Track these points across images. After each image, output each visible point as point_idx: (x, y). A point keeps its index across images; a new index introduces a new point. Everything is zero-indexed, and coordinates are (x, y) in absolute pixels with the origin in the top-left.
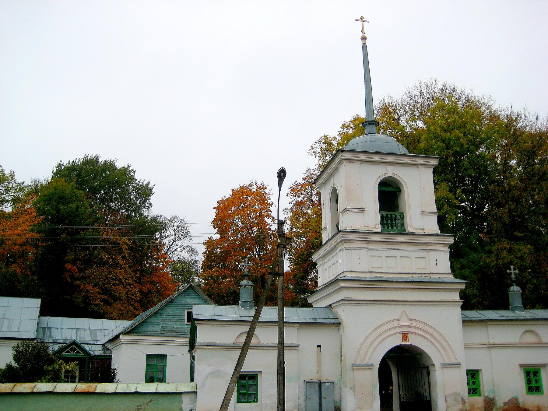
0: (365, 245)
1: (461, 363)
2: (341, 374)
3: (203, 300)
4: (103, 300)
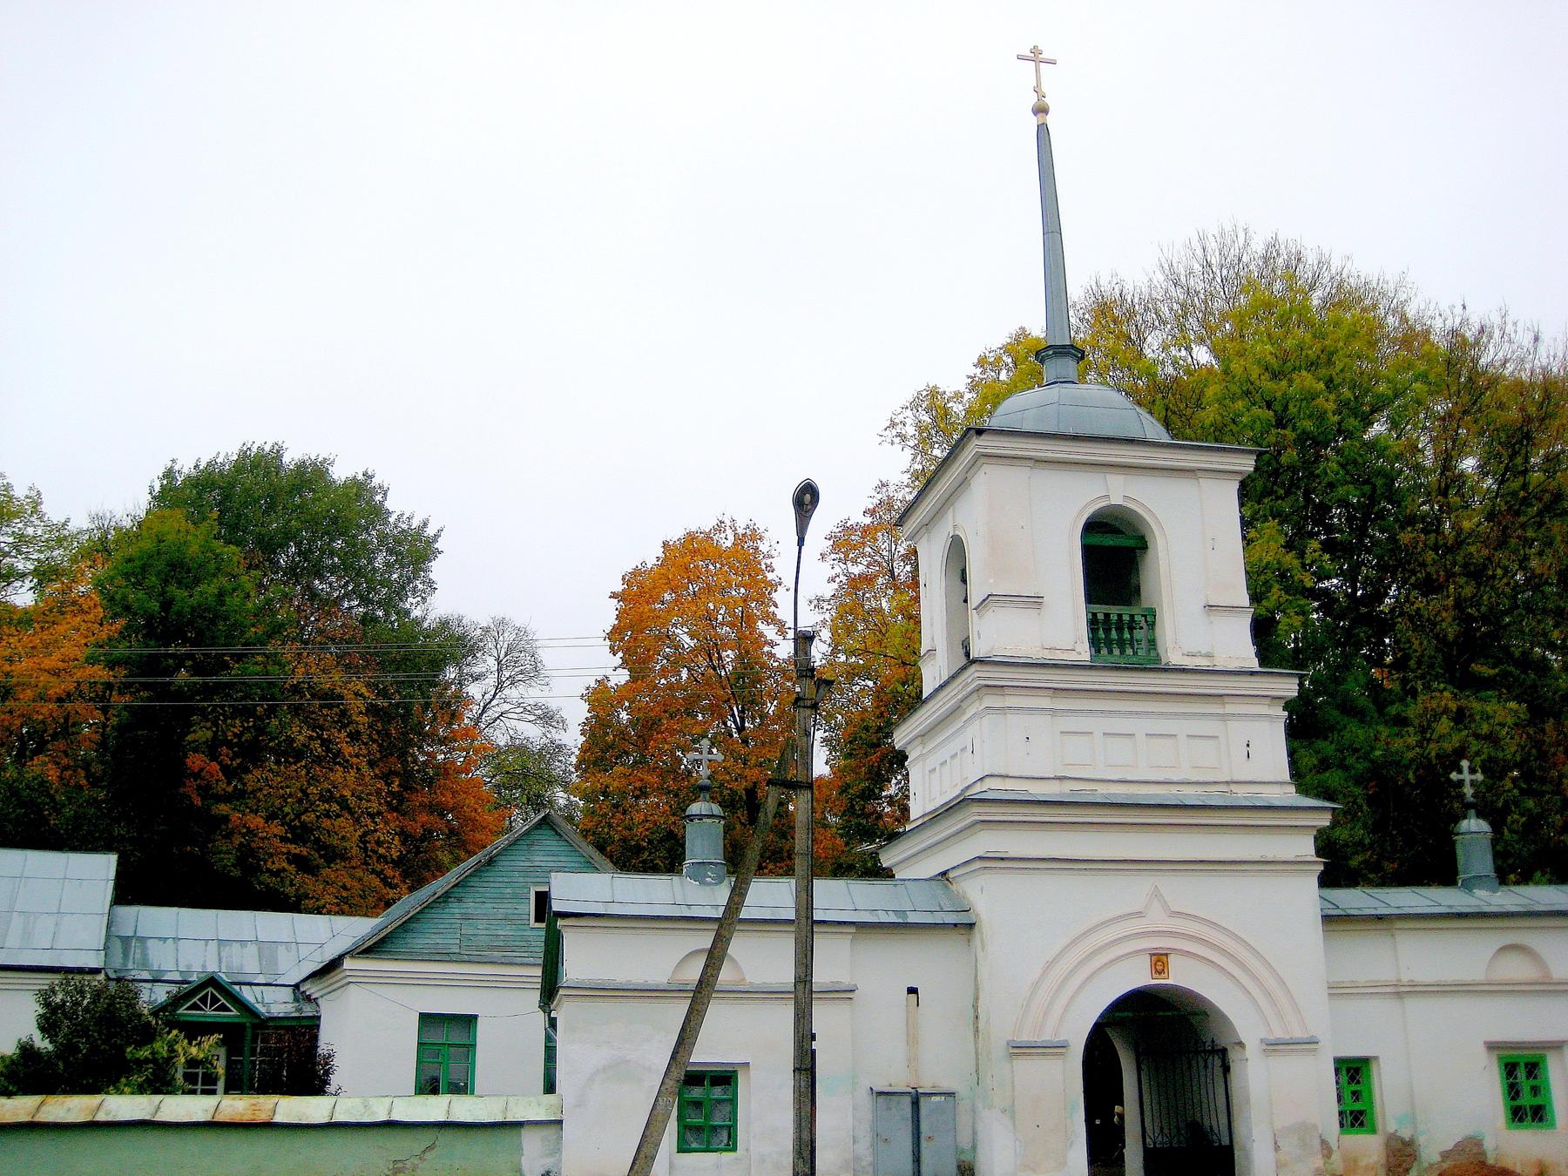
0: (1045, 702)
1: (1320, 1038)
3: (582, 860)
4: (297, 860)
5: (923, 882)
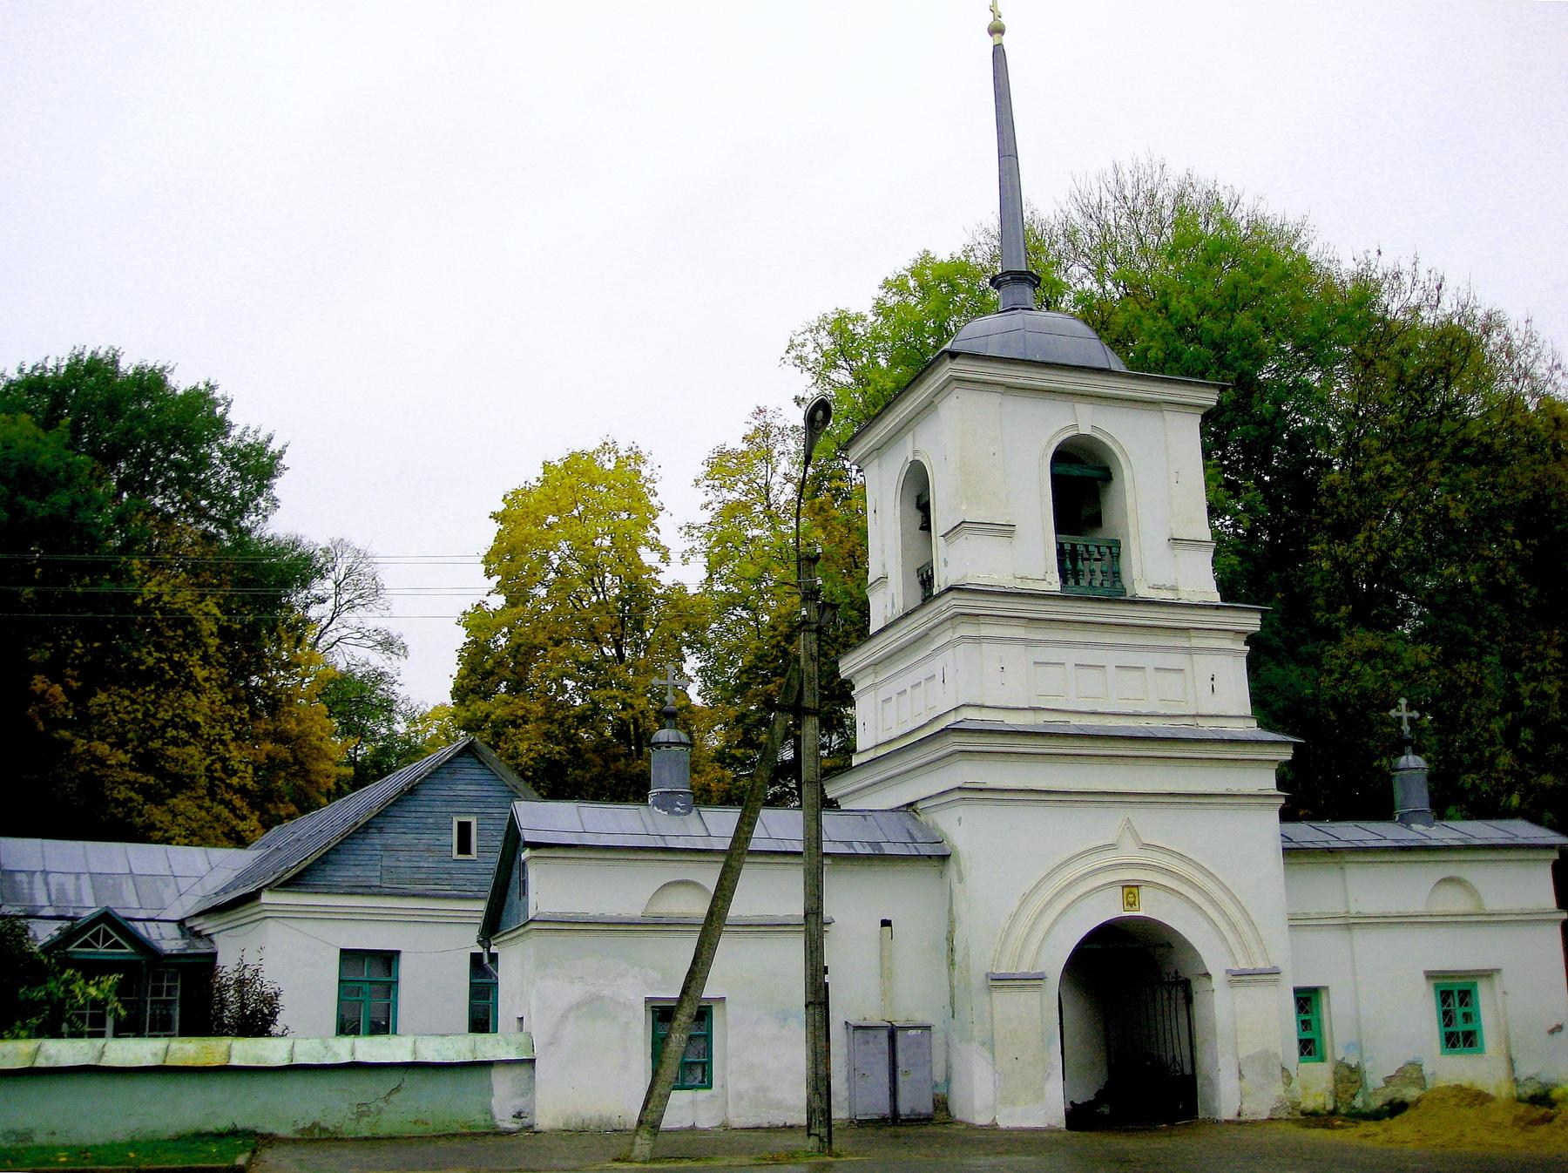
0: (1020, 632)
1: (1281, 968)
2: (952, 1004)
3: (504, 788)
4: (144, 789)
5: (889, 814)
